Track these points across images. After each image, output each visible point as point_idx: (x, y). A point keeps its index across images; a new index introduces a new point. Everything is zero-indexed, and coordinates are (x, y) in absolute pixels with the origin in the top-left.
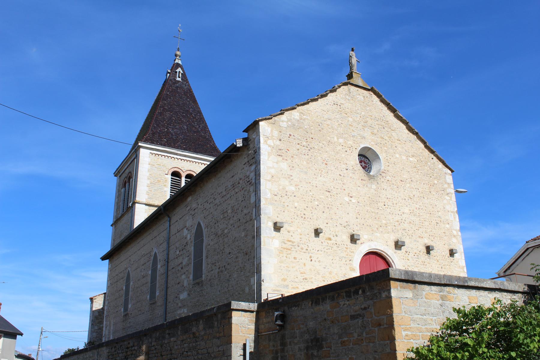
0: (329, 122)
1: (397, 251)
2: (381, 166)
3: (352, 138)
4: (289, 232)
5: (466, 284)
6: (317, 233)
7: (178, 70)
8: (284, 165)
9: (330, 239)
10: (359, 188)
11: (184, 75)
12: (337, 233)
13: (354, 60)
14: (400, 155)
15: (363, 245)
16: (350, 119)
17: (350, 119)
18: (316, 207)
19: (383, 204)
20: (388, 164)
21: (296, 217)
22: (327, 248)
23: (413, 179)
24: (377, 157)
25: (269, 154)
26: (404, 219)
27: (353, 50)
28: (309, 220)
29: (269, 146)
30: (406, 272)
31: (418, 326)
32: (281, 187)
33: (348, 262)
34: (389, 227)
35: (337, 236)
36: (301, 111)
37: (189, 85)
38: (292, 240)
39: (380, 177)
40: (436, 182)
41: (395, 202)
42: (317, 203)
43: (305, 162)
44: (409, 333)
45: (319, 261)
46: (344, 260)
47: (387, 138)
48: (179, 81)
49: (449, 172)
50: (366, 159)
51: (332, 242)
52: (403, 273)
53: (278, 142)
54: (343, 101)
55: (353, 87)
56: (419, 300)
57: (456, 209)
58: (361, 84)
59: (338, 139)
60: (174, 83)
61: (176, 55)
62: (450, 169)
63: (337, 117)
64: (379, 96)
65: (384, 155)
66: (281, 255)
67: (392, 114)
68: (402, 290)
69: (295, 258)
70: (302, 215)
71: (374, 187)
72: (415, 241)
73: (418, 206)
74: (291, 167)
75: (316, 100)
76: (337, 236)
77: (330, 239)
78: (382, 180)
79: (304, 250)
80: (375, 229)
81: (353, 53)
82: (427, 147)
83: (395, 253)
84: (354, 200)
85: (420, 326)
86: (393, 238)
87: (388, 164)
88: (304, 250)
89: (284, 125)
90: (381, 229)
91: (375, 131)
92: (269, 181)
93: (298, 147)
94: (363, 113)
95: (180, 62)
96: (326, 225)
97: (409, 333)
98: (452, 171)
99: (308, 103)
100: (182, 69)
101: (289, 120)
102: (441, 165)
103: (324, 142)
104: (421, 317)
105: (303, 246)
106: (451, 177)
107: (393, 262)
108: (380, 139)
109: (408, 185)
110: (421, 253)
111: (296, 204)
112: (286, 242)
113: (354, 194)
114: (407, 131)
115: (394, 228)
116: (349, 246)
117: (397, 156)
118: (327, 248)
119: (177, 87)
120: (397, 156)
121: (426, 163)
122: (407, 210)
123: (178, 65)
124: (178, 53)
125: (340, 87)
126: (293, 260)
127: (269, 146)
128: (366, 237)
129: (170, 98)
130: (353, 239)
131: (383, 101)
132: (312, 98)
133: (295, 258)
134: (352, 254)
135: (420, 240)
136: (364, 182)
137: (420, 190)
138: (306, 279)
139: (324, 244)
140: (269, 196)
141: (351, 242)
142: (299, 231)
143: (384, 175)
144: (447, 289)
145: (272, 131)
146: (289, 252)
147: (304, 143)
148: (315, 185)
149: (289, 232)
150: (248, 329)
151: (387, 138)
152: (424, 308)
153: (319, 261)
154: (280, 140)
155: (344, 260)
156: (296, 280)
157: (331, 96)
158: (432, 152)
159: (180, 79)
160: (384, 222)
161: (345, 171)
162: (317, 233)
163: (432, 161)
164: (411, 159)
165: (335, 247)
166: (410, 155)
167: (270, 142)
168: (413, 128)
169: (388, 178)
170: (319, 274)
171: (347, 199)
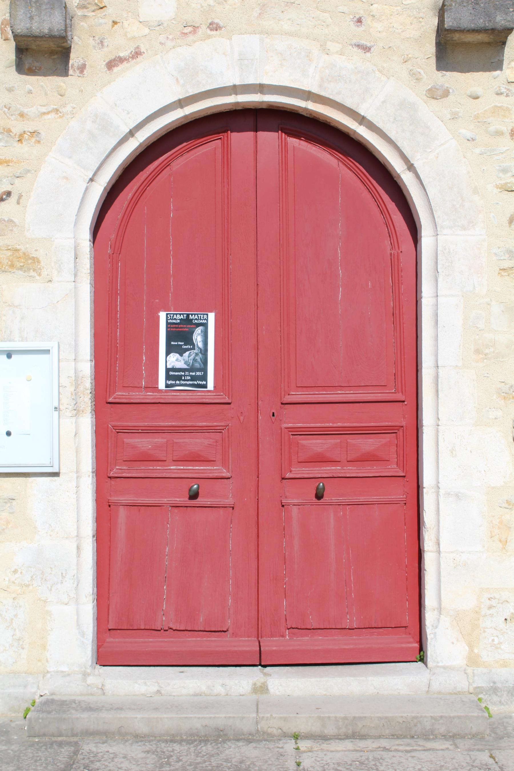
1: (452, 79)
15: (128, 76)
83: (437, 94)
107: (411, 167)
141: (21, 67)
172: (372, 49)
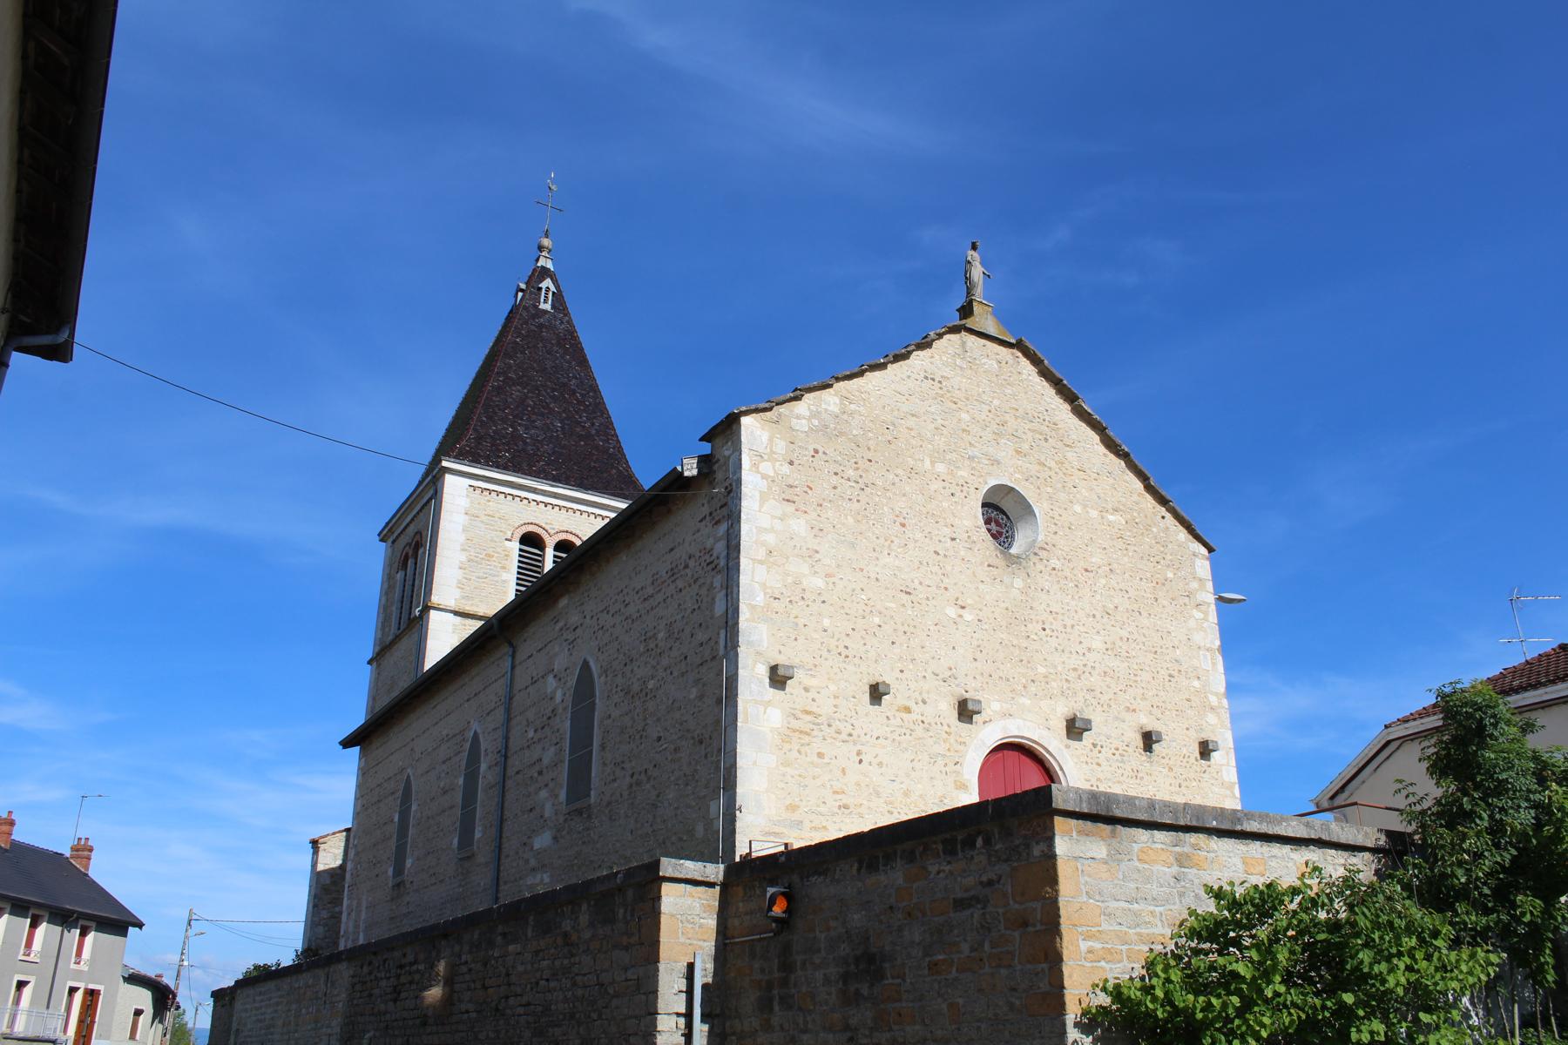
0: (911, 422)
2: (1036, 532)
3: (967, 462)
4: (806, 690)
5: (1239, 828)
6: (877, 693)
7: (543, 285)
8: (799, 525)
9: (908, 710)
10: (981, 586)
11: (558, 298)
12: (925, 696)
13: (977, 272)
14: (1085, 506)
15: (989, 727)
16: (964, 416)
17: (964, 416)
18: (876, 630)
19: (1040, 626)
20: (1054, 528)
21: (825, 654)
22: (899, 731)
23: (1115, 566)
24: (1027, 510)
25: (763, 498)
26: (1090, 664)
27: (974, 247)
28: (857, 660)
29: (764, 477)
30: (1094, 796)
31: (1118, 928)
32: (790, 580)
33: (951, 767)
34: (1054, 684)
35: (924, 702)
36: (844, 393)
37: (570, 322)
38: (814, 709)
39: (1034, 559)
40: (1170, 575)
41: (1069, 623)
42: (877, 620)
43: (851, 520)
44: (1097, 945)
45: (880, 764)
46: (941, 762)
47: (1053, 464)
48: (545, 312)
49: (1204, 551)
50: (1002, 514)
51: (914, 716)
52: (1084, 797)
53: (786, 469)
54: (947, 372)
55: (973, 338)
56: (1123, 866)
57: (1218, 643)
58: (992, 331)
59: (933, 463)
60: (534, 317)
61: (541, 248)
62: (1205, 544)
63: (932, 409)
64: (1035, 361)
65: (1046, 505)
66: (787, 746)
67: (1067, 407)
68: (1083, 838)
69: (820, 755)
70: (841, 649)
71: (1018, 583)
72: (1117, 718)
73: (1125, 634)
74: (815, 531)
75: (882, 366)
76: (924, 702)
77: (908, 710)
78: (1040, 567)
79: (844, 736)
80: (1020, 687)
81: (975, 254)
82: (1149, 488)
83: (1067, 747)
84: (968, 616)
85: (1124, 929)
86: (1062, 710)
87: (1054, 528)
88: (844, 736)
89: (803, 425)
90: (1033, 688)
91: (1026, 447)
92: (761, 562)
93: (835, 480)
94: (996, 402)
95: (550, 265)
96: (900, 675)
97: (1097, 945)
98: (1210, 550)
99: (861, 374)
100: (555, 282)
101: (815, 415)
102: (1183, 535)
103: (899, 471)
104: (1126, 905)
105: (841, 726)
106: (1207, 564)
108: (1037, 467)
109: (1103, 581)
110: (1130, 750)
111: (826, 622)
112: (800, 715)
113: (969, 601)
114: (1102, 449)
115: (1066, 685)
116: (953, 729)
117: (1078, 508)
118: (899, 731)
119: (541, 326)
120: (1078, 508)
121: (1148, 528)
122: (1097, 643)
123: (544, 273)
124: (546, 242)
125: (940, 336)
126: (815, 759)
127: (764, 477)
128: (996, 706)
129: (523, 353)
130: (966, 712)
131: (1045, 373)
132: (872, 362)
133: (820, 755)
134: (962, 748)
135: (1128, 716)
136: (995, 572)
137: (1132, 593)
138: (846, 807)
139: (892, 721)
140: (760, 599)
142: (833, 687)
143: (1043, 554)
144: (1192, 838)
145: (771, 440)
146: (806, 739)
147: (851, 473)
148: (873, 575)
149: (806, 690)
150: (701, 926)
151: (1053, 464)
152: (1133, 885)
153: (880, 764)
154: (791, 463)
155: (941, 762)
156: (823, 809)
157: (919, 359)
158: (1163, 501)
159: (547, 307)
160: (1041, 670)
161: (949, 543)
162: (877, 693)
163: (1162, 524)
164: (1111, 518)
165: (919, 731)
166: (1109, 507)
167: (766, 467)
168: (1118, 441)
169: (1054, 562)
170: (878, 794)
171: (952, 612)
172: (975, 717)
